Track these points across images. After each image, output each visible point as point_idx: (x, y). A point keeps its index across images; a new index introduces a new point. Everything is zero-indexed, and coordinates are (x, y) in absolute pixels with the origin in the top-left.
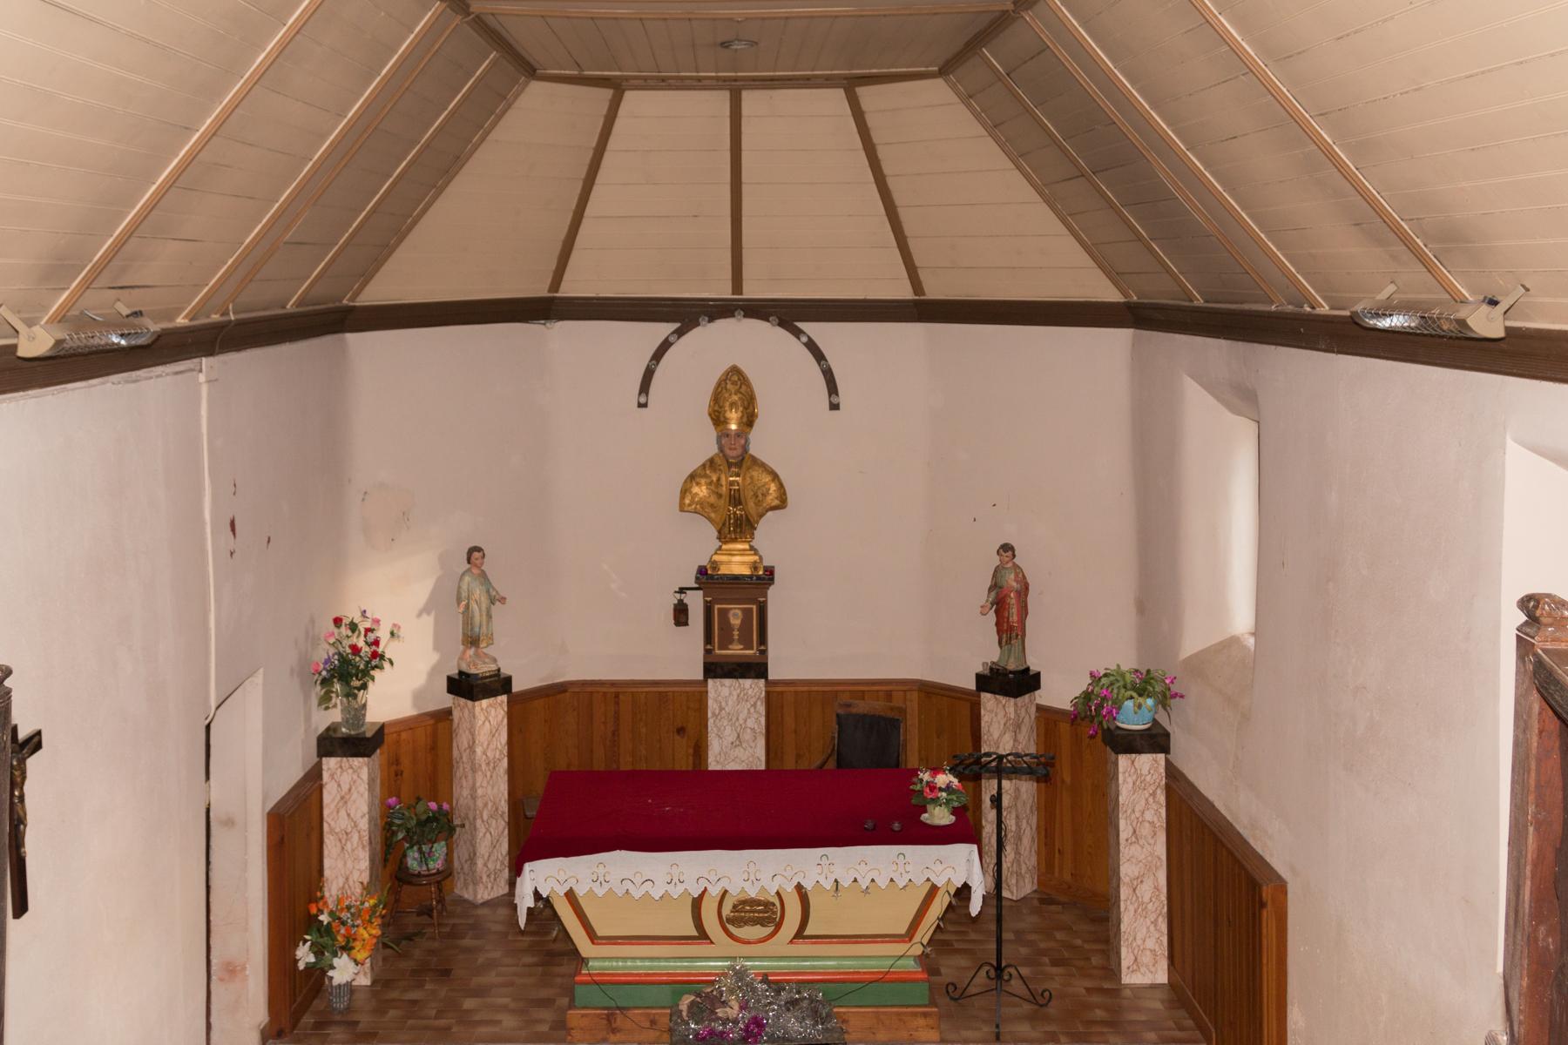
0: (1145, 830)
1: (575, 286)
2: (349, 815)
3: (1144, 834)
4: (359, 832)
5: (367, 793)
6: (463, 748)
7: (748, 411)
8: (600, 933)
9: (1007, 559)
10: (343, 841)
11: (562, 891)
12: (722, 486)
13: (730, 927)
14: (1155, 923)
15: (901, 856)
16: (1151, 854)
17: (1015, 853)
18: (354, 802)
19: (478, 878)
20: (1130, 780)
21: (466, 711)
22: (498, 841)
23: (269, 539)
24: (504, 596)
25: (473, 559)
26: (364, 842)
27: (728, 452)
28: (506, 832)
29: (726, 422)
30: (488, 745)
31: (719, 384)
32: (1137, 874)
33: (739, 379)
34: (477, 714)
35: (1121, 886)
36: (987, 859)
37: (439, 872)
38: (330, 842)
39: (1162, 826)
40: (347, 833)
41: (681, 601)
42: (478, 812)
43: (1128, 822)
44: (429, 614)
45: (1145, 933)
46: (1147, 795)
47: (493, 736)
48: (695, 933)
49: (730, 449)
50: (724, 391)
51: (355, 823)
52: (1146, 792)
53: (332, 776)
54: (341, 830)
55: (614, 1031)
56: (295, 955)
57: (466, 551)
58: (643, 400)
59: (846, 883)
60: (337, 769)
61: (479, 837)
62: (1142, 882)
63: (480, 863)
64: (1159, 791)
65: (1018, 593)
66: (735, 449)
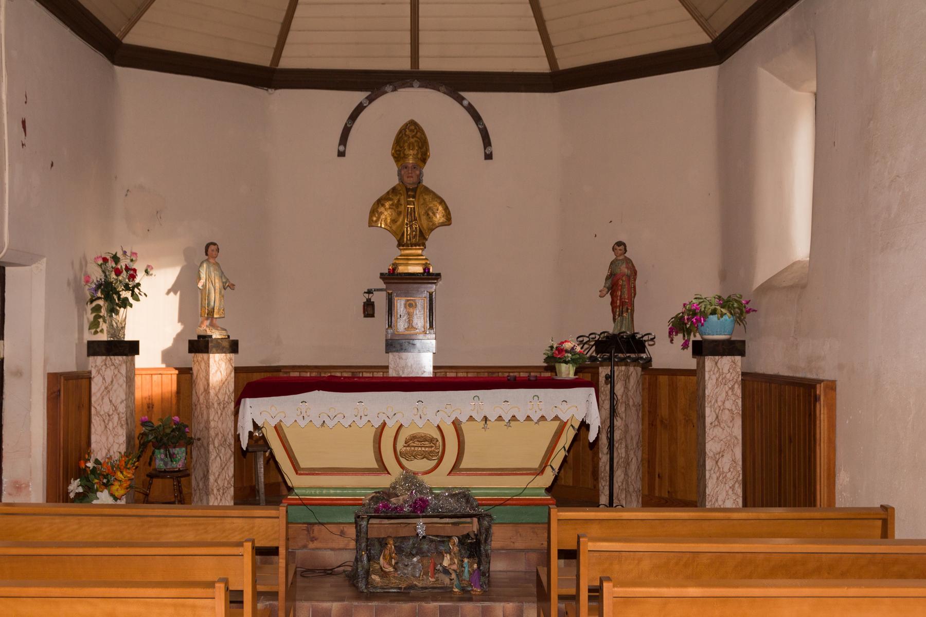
0: (726, 416)
1: (291, 60)
2: (111, 401)
3: (725, 419)
4: (119, 414)
5: (125, 384)
6: (200, 393)
7: (423, 150)
8: (303, 464)
9: (620, 252)
10: (106, 422)
11: (273, 423)
12: (401, 205)
13: (401, 459)
14: (733, 488)
15: (536, 398)
16: (730, 435)
17: (625, 475)
18: (115, 391)
19: (211, 404)
20: (714, 377)
21: (202, 450)
22: (226, 465)
23: (52, 163)
24: (233, 283)
25: (210, 250)
26: (122, 422)
27: (406, 179)
28: (232, 459)
29: (405, 157)
30: (219, 475)
31: (400, 132)
32: (718, 450)
33: (415, 128)
34: (211, 450)
35: (707, 459)
36: (602, 397)
37: (179, 471)
38: (96, 422)
39: (739, 413)
40: (109, 415)
41: (369, 300)
42: (211, 439)
43: (712, 409)
44: (175, 293)
45: (724, 396)
46: (727, 389)
47: (223, 469)
48: (374, 465)
49: (408, 177)
50: (404, 136)
51: (115, 407)
52: (726, 386)
53: (98, 372)
54: (105, 413)
55: (313, 539)
56: (68, 490)
57: (205, 245)
58: (342, 148)
59: (492, 417)
60: (102, 366)
61: (212, 459)
62: (723, 456)
63: (212, 478)
64: (736, 386)
65: (629, 277)
66: (412, 177)
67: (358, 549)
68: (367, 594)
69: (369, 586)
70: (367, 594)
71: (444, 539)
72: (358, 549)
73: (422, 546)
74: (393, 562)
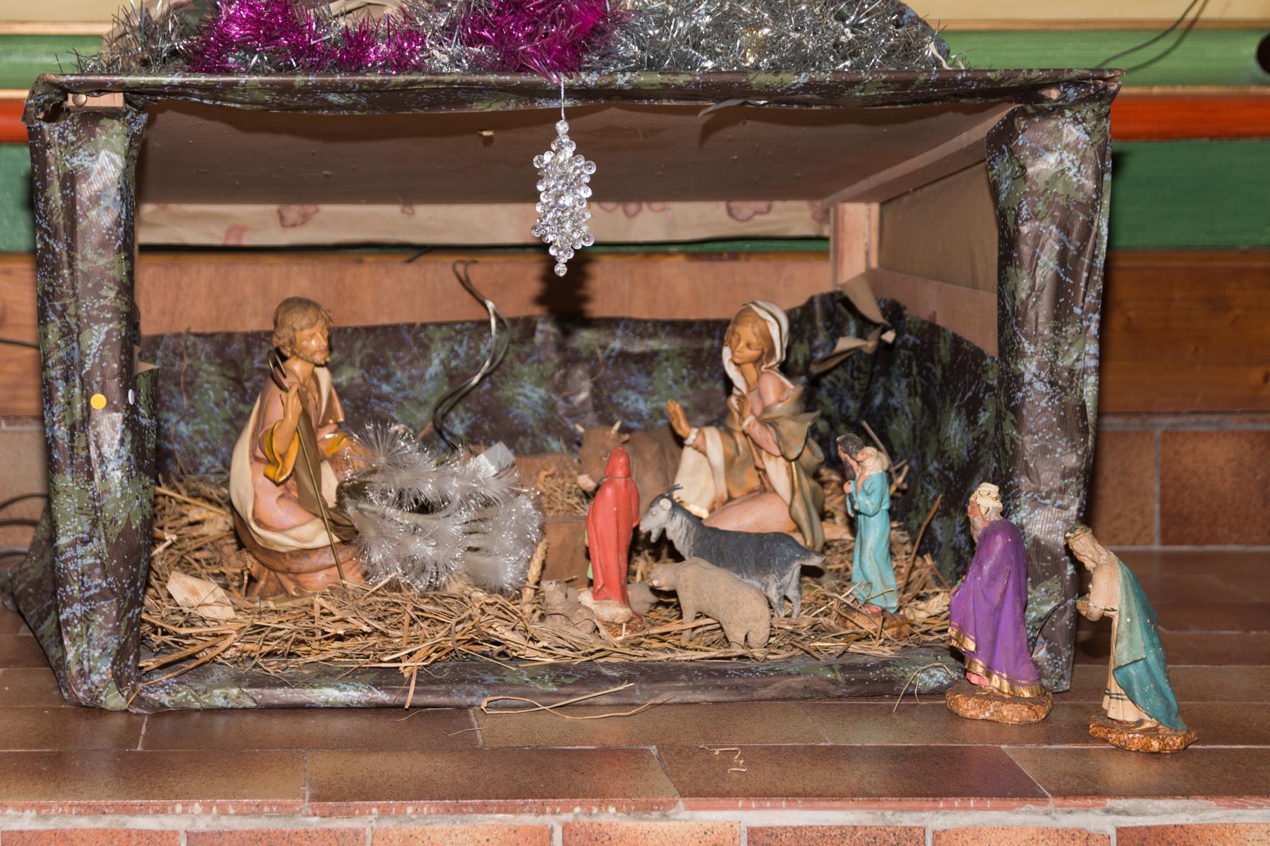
67: (56, 372)
68: (132, 729)
69: (149, 663)
70: (132, 729)
71: (653, 344)
72: (56, 372)
73: (506, 392)
74: (330, 483)
